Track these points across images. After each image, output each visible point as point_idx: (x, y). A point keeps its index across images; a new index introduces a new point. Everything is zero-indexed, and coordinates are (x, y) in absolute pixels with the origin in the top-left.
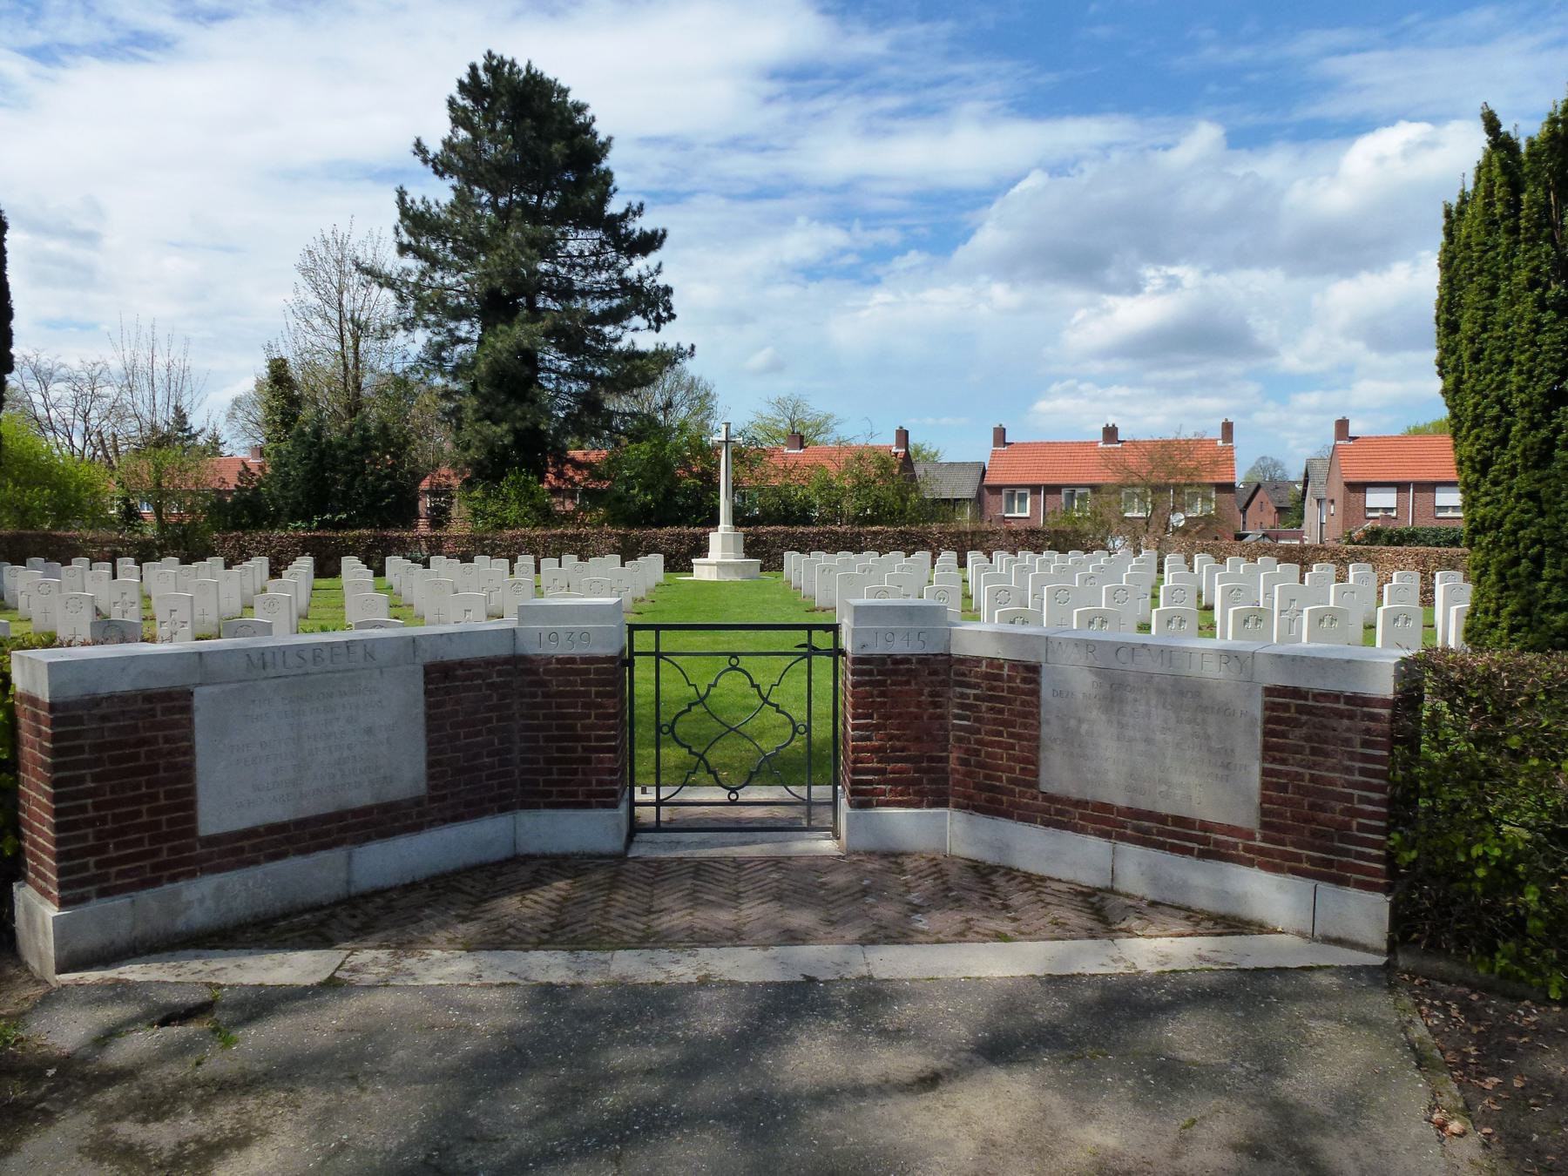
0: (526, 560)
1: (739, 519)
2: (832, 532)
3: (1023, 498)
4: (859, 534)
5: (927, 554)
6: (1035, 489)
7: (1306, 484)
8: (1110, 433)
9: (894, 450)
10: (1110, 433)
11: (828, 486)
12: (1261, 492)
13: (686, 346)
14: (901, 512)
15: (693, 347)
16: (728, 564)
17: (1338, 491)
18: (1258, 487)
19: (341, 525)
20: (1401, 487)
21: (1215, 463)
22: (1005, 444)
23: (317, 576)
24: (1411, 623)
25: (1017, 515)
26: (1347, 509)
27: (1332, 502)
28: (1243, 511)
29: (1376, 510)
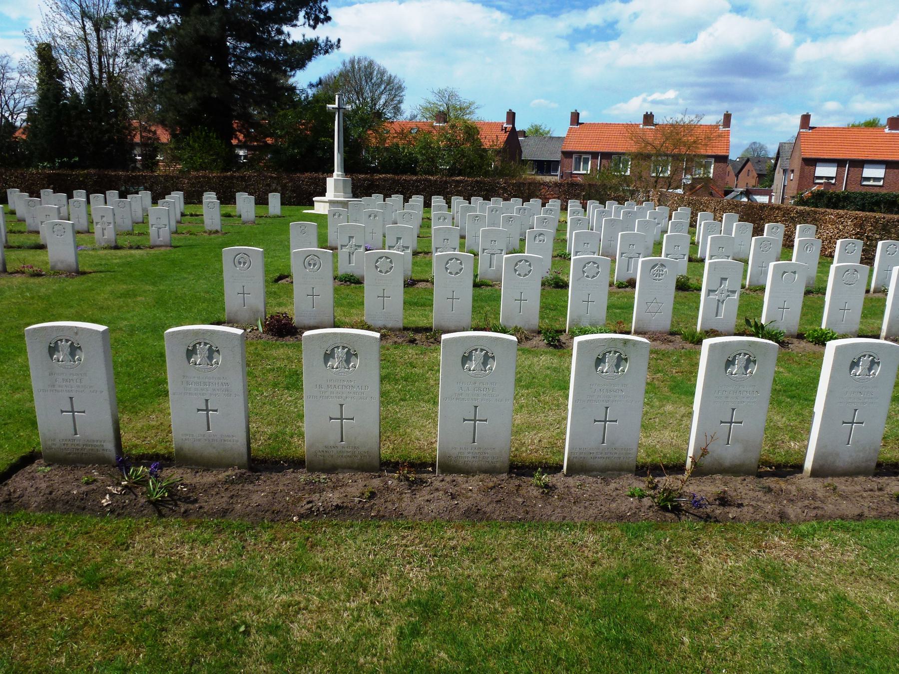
0: (80, 196)
1: (348, 169)
2: (426, 180)
3: (586, 162)
4: (446, 182)
5: (539, 201)
6: (595, 155)
7: (777, 159)
8: (648, 118)
9: (505, 125)
10: (648, 118)
11: (427, 146)
12: (749, 163)
13: (334, 40)
14: (480, 167)
15: (339, 41)
16: (337, 202)
17: (797, 164)
18: (748, 160)
19: (73, 166)
20: (840, 163)
21: (708, 138)
22: (578, 124)
23: (186, 203)
24: (878, 370)
25: (582, 172)
26: (802, 177)
27: (793, 171)
28: (737, 175)
29: (821, 178)
